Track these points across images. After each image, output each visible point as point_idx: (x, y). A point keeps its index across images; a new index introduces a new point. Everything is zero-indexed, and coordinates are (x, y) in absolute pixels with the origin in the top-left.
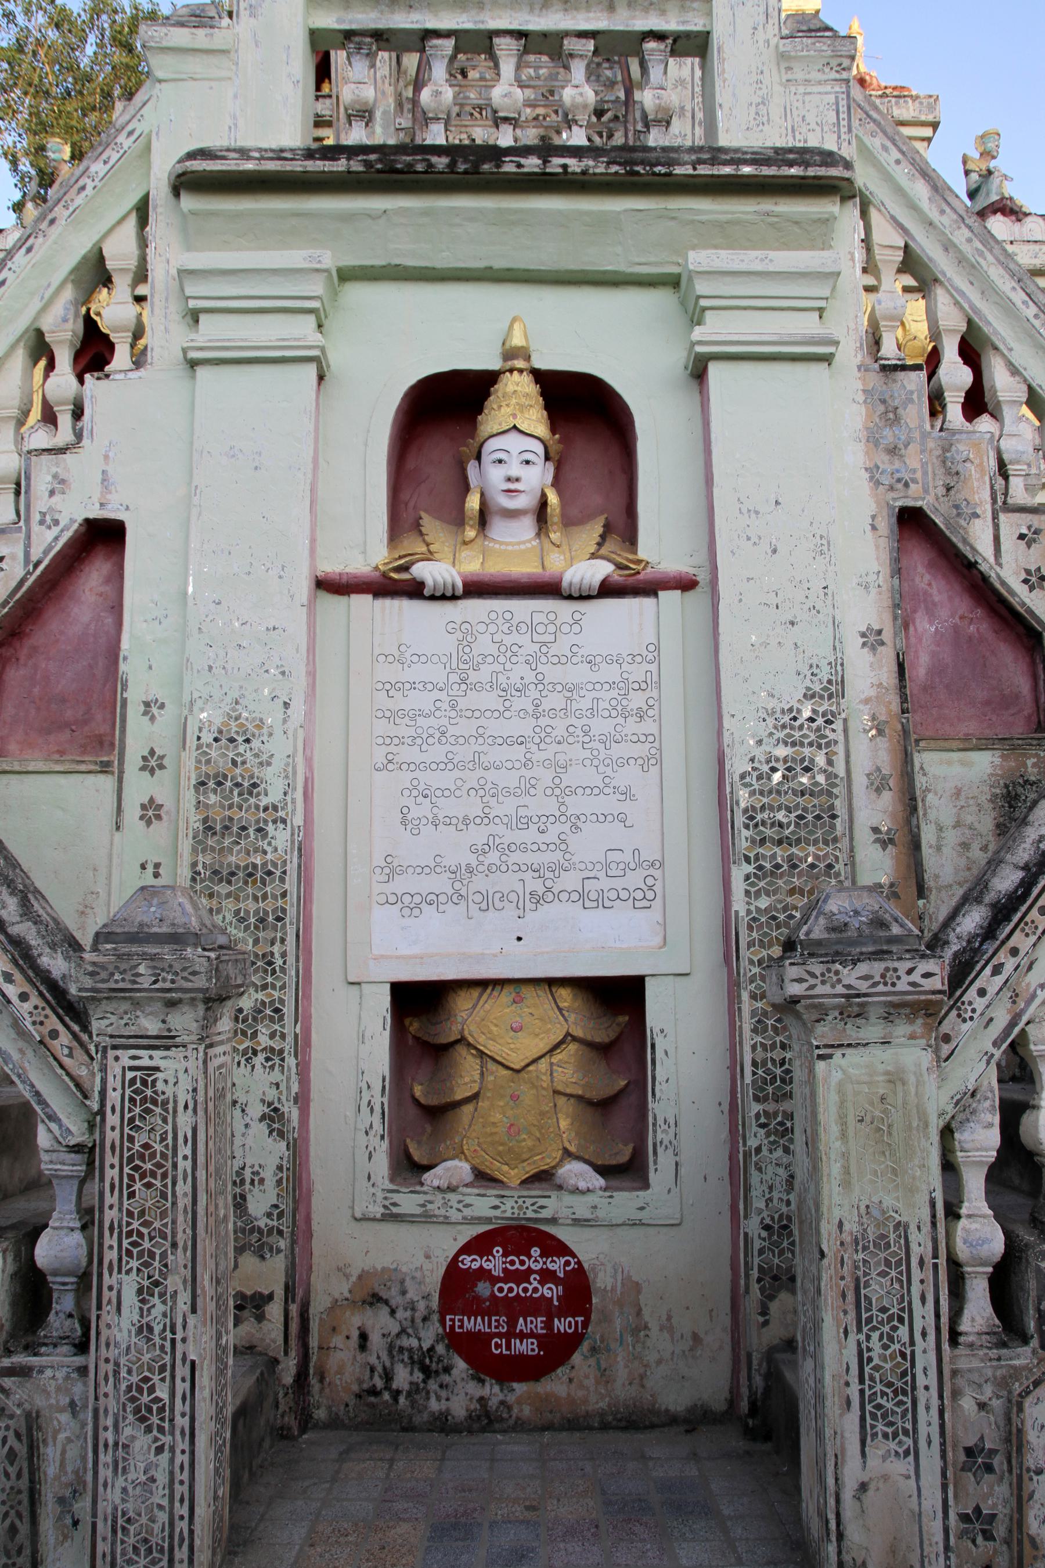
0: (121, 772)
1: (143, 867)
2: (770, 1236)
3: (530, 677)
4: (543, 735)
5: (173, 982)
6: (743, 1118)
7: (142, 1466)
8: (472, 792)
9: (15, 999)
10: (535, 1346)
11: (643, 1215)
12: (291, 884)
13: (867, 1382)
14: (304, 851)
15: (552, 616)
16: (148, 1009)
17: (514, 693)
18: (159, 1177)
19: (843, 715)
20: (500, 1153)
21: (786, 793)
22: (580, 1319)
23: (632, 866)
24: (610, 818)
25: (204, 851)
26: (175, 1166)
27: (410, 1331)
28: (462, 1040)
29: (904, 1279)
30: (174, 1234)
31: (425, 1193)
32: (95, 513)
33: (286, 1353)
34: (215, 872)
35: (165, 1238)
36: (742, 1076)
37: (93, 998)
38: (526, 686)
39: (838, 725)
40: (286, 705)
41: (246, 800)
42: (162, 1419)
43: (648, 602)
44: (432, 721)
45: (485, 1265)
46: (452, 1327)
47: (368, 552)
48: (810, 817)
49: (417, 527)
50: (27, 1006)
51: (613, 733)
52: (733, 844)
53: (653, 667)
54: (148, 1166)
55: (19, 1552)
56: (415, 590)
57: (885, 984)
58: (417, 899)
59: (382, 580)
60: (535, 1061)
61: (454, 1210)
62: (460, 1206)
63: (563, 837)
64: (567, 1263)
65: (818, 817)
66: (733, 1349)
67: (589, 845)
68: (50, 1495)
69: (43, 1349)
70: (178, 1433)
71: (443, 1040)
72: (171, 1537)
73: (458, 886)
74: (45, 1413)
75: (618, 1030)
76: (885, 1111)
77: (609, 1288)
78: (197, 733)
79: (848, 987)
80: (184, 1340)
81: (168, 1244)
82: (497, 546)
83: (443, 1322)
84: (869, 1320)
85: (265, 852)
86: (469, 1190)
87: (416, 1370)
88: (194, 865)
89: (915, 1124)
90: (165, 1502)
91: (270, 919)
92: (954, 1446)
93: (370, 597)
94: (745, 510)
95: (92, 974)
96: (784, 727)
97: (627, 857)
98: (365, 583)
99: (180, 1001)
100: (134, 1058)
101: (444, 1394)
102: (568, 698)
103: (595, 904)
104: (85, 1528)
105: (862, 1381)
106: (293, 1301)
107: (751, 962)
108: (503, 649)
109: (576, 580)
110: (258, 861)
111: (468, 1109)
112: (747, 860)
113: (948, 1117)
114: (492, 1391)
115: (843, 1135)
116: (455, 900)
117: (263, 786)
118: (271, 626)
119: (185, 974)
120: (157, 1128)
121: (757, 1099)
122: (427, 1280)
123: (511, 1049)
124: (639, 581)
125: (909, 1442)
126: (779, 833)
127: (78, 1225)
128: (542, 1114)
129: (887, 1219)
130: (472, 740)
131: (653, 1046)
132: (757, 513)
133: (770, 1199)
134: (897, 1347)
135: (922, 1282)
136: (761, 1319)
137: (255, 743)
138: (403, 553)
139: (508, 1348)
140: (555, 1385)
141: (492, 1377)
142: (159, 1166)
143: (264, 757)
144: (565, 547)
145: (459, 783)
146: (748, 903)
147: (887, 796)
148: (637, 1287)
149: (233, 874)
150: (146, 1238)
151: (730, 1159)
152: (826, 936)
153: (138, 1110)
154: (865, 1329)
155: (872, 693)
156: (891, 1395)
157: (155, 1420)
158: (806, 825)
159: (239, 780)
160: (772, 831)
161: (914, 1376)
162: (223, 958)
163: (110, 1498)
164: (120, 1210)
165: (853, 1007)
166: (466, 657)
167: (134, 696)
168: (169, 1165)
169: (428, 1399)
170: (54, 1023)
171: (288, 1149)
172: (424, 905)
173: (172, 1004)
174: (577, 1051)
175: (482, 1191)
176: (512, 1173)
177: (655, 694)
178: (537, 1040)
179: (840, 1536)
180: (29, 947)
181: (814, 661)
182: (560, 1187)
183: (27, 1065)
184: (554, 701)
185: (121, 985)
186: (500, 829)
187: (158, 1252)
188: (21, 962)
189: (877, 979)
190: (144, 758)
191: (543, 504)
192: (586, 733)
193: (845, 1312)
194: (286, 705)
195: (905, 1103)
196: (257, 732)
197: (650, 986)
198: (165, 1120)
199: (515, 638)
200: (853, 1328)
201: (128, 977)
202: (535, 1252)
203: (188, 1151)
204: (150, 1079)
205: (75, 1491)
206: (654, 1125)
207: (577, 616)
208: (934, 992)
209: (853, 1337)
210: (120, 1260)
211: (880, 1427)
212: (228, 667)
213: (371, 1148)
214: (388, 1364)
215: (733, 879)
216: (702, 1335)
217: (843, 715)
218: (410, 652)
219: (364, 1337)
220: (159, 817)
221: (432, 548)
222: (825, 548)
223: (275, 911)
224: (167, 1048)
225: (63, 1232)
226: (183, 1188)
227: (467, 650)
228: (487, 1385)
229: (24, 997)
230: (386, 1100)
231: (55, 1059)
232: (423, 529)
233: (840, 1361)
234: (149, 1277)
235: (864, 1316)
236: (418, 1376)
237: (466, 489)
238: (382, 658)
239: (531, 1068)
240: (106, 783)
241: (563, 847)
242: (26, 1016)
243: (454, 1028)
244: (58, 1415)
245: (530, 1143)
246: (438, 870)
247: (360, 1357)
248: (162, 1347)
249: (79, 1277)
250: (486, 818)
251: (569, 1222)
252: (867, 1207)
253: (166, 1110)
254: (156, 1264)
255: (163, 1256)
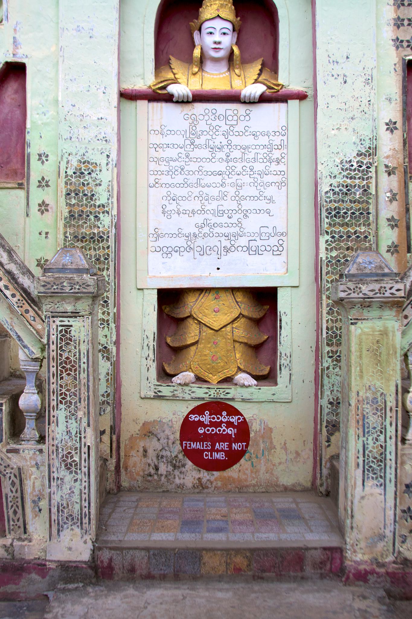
0: (28, 188)
1: (40, 234)
2: (332, 406)
3: (225, 142)
4: (231, 171)
5: (79, 289)
6: (322, 353)
7: (68, 487)
8: (196, 198)
9: (9, 296)
10: (223, 456)
11: (275, 398)
12: (111, 242)
13: (366, 457)
14: (118, 226)
15: (235, 112)
16: (67, 301)
17: (217, 150)
18: (73, 371)
19: (376, 164)
20: (208, 369)
21: (346, 202)
22: (244, 444)
23: (273, 235)
24: (262, 211)
25: (70, 227)
26: (80, 366)
27: (166, 448)
28: (190, 316)
29: (384, 416)
30: (80, 394)
31: (174, 386)
32: (10, 59)
33: (111, 457)
34: (75, 237)
35: (76, 396)
36: (322, 334)
37: (44, 296)
38: (222, 147)
39: (373, 169)
40: (108, 156)
41: (89, 202)
42: (76, 469)
43: (283, 105)
44: (177, 164)
45: (201, 419)
46: (186, 447)
47: (144, 78)
48: (357, 213)
49: (168, 63)
50: (15, 300)
51: (264, 170)
52: (321, 226)
53: (285, 138)
54: (69, 366)
55: (18, 520)
56: (169, 98)
57: (380, 293)
58: (170, 249)
59: (153, 93)
60: (225, 326)
61: (187, 394)
62: (190, 392)
63: (240, 220)
64: (239, 419)
65: (361, 214)
66: (314, 458)
67: (252, 224)
68: (29, 500)
69: (23, 442)
70: (83, 474)
71: (182, 316)
72: (81, 514)
73: (189, 243)
74: (25, 468)
75: (264, 312)
76: (379, 347)
77: (258, 430)
78: (65, 170)
79: (364, 294)
80: (85, 437)
81: (77, 399)
82: (209, 76)
83: (181, 444)
84: (368, 432)
85: (99, 227)
86: (194, 385)
87: (169, 466)
88: (65, 233)
89: (391, 353)
90: (79, 501)
91: (102, 259)
92: (401, 484)
93: (146, 102)
94: (331, 61)
95: (44, 286)
96: (347, 169)
97: (270, 230)
98: (144, 95)
99: (81, 297)
100: (61, 321)
101: (182, 476)
102: (243, 153)
103: (254, 253)
104: (45, 513)
105: (364, 456)
106: (114, 434)
107: (327, 281)
108: (212, 128)
109: (247, 95)
110: (96, 231)
111: (193, 348)
112: (327, 233)
113: (406, 350)
114: (205, 475)
115: (361, 357)
116: (188, 250)
117: (97, 195)
118: (100, 117)
119: (84, 286)
120: (72, 351)
121: (328, 345)
122: (174, 426)
123: (214, 321)
124: (278, 95)
125: (382, 481)
126: (342, 221)
127: (36, 392)
128: (228, 351)
129: (377, 391)
130: (196, 173)
131: (281, 321)
132: (337, 62)
133: (333, 391)
134: (379, 443)
135: (391, 417)
136: (327, 444)
137: (94, 175)
138: (162, 80)
139: (211, 456)
140: (233, 472)
141: (204, 469)
142: (73, 366)
143: (98, 182)
144: (243, 76)
145: (190, 194)
146: (327, 254)
147: (395, 203)
148: (271, 430)
149: (84, 237)
150: (68, 396)
151: (315, 372)
152: (356, 272)
153: (64, 343)
154: (366, 436)
155: (390, 153)
156: (376, 462)
157: (73, 469)
158: (356, 217)
159: (86, 193)
160: (341, 215)
161: (385, 455)
162: (99, 279)
163: (56, 499)
164: (57, 384)
165: (366, 303)
166: (193, 132)
167: (33, 150)
168: (77, 366)
169: (175, 478)
170: (26, 306)
171: (111, 365)
172: (173, 253)
173: (78, 299)
174: (245, 322)
175: (200, 386)
176: (214, 378)
177: (285, 151)
178: (226, 316)
179: (352, 516)
180: (14, 274)
181: (362, 138)
182: (236, 384)
183: (14, 324)
184: (236, 154)
185: (56, 291)
186: (210, 216)
187: (73, 402)
188: (12, 281)
189: (377, 291)
190: (39, 182)
191: (232, 52)
192: (251, 170)
193: (358, 429)
194: (108, 156)
195: (387, 344)
196: (94, 170)
197: (280, 294)
198: (75, 347)
199: (217, 122)
200: (361, 435)
201: (59, 287)
202: (224, 413)
203: (85, 361)
204: (68, 330)
205: (39, 498)
206: (280, 356)
207: (248, 112)
208: (401, 297)
209: (361, 439)
210: (57, 405)
211: (371, 475)
212: (80, 137)
213: (148, 366)
214: (156, 463)
215: (320, 242)
216: (300, 452)
217: (376, 164)
218: (166, 129)
219: (145, 451)
220: (47, 210)
221: (177, 76)
222: (370, 81)
223: (104, 255)
224: (76, 317)
225: (30, 395)
226: (83, 375)
227: (194, 128)
228: (202, 472)
229: (13, 296)
230: (155, 344)
231: (28, 322)
232: (172, 66)
233: (355, 448)
234: (70, 412)
235: (366, 430)
236: (170, 468)
237: (194, 46)
238: (152, 132)
239: (223, 329)
240: (21, 193)
241: (240, 225)
242: (15, 303)
243: (187, 311)
244: (31, 469)
245: (222, 364)
246: (180, 235)
247: (144, 460)
248: (76, 441)
249: (37, 414)
250: (203, 211)
251: (240, 400)
252: (370, 386)
253: (75, 343)
254: (73, 407)
255: (76, 403)
